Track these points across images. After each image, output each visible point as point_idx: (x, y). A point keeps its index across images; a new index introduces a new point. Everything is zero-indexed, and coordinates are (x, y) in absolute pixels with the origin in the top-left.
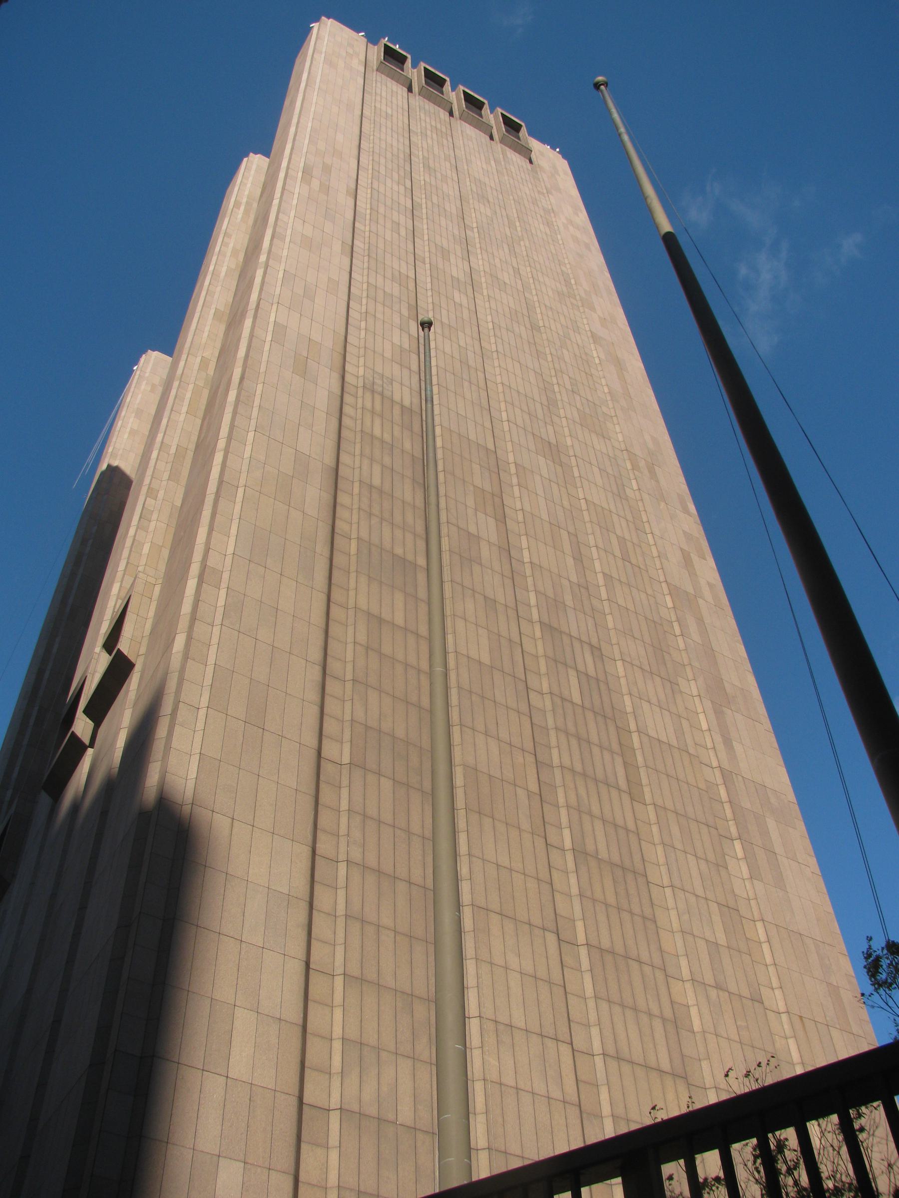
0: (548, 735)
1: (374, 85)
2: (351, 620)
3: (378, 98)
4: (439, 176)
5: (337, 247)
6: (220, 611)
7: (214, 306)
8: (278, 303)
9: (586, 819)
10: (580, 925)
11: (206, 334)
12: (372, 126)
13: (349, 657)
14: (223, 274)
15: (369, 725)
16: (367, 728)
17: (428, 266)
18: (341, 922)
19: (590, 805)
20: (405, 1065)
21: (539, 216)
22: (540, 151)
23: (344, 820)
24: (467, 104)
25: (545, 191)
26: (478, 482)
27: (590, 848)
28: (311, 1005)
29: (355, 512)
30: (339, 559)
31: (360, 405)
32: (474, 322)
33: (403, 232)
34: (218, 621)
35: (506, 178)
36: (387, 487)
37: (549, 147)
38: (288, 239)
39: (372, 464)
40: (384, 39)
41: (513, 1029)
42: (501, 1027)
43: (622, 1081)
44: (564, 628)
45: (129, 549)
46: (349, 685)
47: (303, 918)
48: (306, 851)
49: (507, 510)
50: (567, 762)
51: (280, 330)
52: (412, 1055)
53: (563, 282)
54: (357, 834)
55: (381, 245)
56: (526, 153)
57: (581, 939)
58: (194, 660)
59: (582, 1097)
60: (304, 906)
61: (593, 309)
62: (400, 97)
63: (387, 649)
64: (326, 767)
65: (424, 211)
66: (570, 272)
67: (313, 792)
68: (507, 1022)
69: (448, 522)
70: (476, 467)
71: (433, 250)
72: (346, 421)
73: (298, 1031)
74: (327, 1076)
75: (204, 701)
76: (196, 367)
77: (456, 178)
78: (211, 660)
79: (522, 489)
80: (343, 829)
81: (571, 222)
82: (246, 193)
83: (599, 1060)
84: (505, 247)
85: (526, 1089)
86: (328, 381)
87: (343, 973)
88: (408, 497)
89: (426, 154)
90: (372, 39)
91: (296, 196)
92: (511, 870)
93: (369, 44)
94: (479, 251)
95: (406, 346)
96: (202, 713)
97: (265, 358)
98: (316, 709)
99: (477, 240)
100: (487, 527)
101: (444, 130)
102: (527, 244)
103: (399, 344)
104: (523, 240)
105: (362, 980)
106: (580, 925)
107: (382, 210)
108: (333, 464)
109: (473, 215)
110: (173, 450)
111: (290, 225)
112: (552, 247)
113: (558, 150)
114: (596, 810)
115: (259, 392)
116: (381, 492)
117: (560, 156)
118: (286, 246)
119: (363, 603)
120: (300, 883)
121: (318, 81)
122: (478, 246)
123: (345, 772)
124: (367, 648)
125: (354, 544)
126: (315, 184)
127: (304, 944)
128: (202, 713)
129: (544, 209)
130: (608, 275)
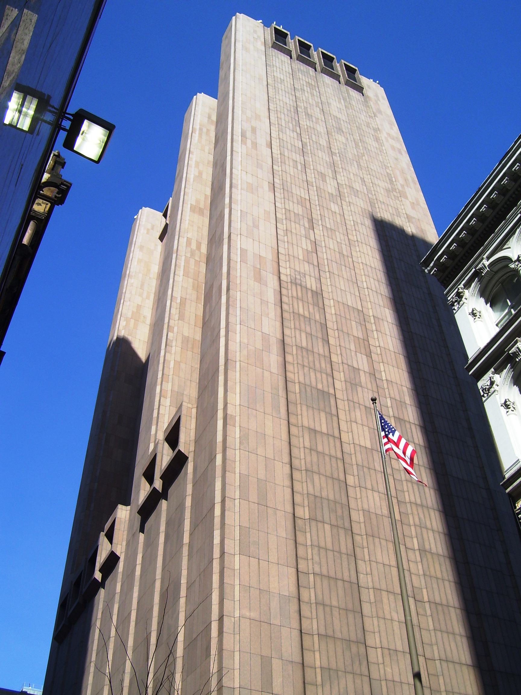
0: (402, 485)
1: (271, 59)
2: (301, 434)
3: (275, 69)
4: (314, 119)
5: (266, 186)
6: (238, 441)
7: (189, 203)
8: (241, 234)
9: (424, 531)
10: (425, 591)
11: (187, 222)
12: (274, 90)
13: (302, 456)
14: (192, 180)
15: (316, 495)
16: (315, 497)
17: (315, 188)
18: (314, 606)
19: (426, 523)
20: (350, 677)
21: (371, 136)
22: (367, 85)
23: (309, 550)
24: (324, 59)
25: (373, 115)
26: (355, 334)
27: (427, 547)
28: (304, 651)
29: (295, 365)
30: (291, 397)
31: (290, 295)
32: (343, 223)
33: (299, 168)
34: (237, 447)
35: (351, 110)
36: (310, 347)
37: (372, 80)
38: (239, 187)
39: (301, 333)
40: (273, 23)
41: (397, 652)
42: (392, 652)
43: (449, 672)
44: (406, 418)
45: (162, 364)
46: (304, 472)
47: (296, 607)
48: (294, 570)
49: (371, 347)
50: (413, 499)
51: (243, 252)
52: (352, 672)
53: (388, 182)
54: (316, 558)
55: (289, 180)
56: (360, 89)
57: (426, 599)
58: (229, 472)
59: (431, 682)
60: (296, 601)
61: (406, 198)
62: (286, 64)
63: (320, 449)
64: (299, 522)
65: (309, 148)
66: (392, 173)
67: (293, 538)
68: (394, 649)
69: (342, 363)
70: (354, 323)
71: (317, 176)
72: (285, 307)
73: (300, 666)
74: (315, 687)
75: (237, 496)
76: (185, 244)
77: (323, 119)
78: (237, 471)
79: (379, 333)
80: (310, 557)
81: (388, 134)
82: (199, 121)
83: (438, 662)
84: (355, 163)
85: (405, 682)
86: (272, 282)
87: (317, 633)
88: (321, 352)
89: (305, 105)
90: (267, 24)
91: (240, 154)
92: (390, 566)
93: (265, 27)
94: (341, 170)
95: (310, 249)
96: (237, 502)
97: (238, 275)
98: (290, 490)
99: (339, 163)
100: (362, 362)
101: (313, 84)
102: (367, 159)
103: (306, 248)
104: (364, 156)
105: (326, 636)
106: (425, 591)
107: (286, 154)
108: (281, 338)
109: (336, 144)
110: (179, 301)
111: (239, 176)
112: (380, 157)
113: (377, 82)
114: (429, 525)
115: (238, 298)
116: (307, 350)
117: (379, 85)
118: (239, 192)
119: (306, 424)
120: (293, 589)
121: (241, 64)
122: (340, 166)
123: (307, 524)
124: (311, 449)
125: (297, 386)
126: (249, 142)
127: (298, 621)
128: (237, 502)
129: (374, 129)
130: (412, 169)
